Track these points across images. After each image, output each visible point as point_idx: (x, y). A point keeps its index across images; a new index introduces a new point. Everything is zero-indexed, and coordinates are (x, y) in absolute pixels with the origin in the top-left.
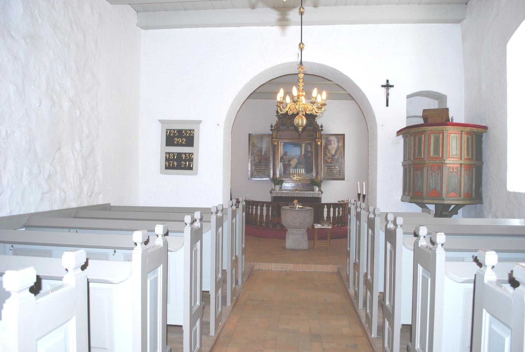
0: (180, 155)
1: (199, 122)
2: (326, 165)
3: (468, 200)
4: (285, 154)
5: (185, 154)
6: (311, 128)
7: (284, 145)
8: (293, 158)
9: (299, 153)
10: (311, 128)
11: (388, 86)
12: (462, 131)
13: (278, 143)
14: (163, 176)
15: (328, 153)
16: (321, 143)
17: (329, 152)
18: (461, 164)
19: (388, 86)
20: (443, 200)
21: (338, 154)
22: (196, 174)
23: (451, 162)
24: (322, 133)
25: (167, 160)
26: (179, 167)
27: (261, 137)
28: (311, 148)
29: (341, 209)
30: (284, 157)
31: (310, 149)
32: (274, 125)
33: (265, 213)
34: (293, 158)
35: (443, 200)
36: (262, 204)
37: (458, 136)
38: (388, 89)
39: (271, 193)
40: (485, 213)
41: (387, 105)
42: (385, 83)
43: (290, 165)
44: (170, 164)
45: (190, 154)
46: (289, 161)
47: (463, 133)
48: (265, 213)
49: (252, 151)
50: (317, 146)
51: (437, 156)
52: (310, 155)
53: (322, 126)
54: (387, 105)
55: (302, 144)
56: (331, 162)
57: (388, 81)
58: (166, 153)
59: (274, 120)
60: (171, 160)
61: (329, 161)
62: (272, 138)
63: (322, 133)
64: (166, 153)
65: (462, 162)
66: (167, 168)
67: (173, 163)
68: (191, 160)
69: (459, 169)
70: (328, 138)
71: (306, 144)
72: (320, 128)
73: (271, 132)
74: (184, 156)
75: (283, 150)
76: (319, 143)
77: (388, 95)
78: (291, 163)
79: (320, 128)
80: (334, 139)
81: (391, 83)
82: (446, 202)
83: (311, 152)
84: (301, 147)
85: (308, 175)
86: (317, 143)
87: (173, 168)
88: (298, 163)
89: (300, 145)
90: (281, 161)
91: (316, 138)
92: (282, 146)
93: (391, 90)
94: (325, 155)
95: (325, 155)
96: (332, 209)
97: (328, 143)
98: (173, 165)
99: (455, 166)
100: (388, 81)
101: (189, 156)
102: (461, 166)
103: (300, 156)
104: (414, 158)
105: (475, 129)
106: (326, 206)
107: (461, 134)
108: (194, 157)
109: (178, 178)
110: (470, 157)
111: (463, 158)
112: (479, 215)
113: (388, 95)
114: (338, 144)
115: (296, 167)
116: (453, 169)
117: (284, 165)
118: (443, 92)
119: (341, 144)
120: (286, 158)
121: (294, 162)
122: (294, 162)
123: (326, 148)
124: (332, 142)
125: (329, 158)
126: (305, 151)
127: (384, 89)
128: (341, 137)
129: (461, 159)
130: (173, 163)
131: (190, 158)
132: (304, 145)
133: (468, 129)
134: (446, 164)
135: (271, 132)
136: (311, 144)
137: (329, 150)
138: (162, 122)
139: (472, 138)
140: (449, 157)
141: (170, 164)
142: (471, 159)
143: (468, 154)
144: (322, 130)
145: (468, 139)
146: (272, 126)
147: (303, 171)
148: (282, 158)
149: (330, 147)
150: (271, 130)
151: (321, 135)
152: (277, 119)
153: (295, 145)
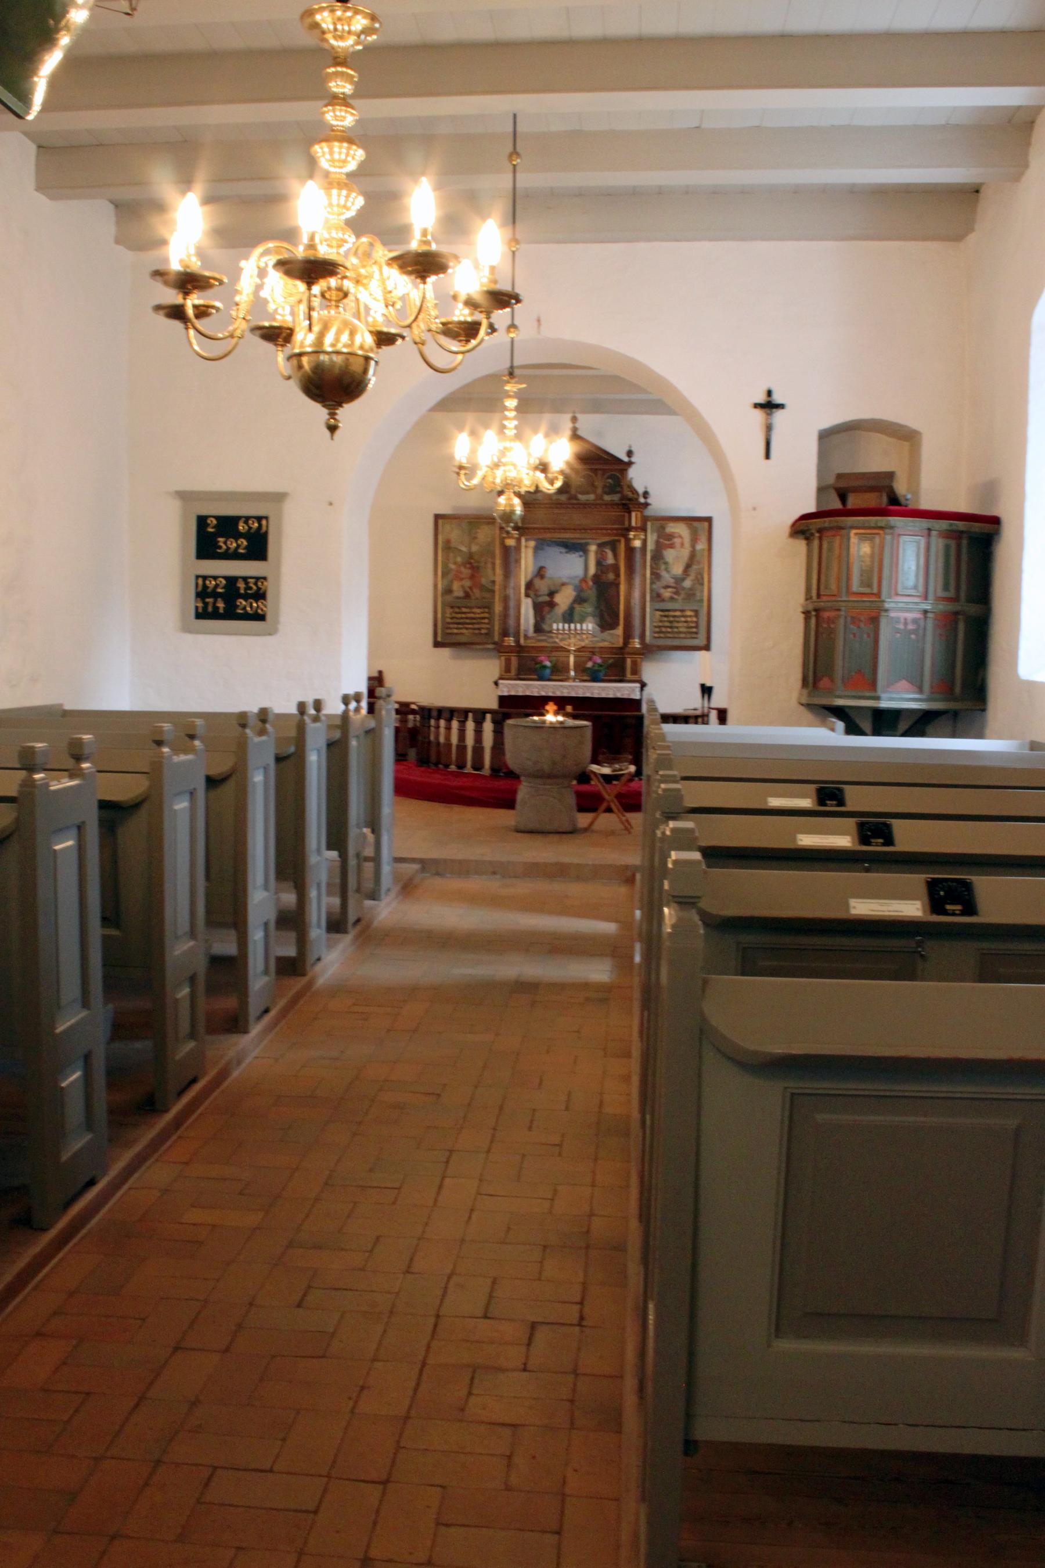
0: (232, 581)
1: (279, 498)
3: (943, 700)
4: (540, 573)
5: (245, 579)
6: (616, 498)
8: (563, 584)
10: (616, 498)
11: (769, 406)
12: (929, 530)
13: (519, 540)
14: (189, 637)
15: (664, 574)
16: (644, 542)
17: (667, 570)
18: (925, 612)
19: (769, 406)
20: (878, 698)
21: (692, 576)
22: (272, 632)
23: (901, 605)
24: (648, 512)
25: (202, 594)
26: (231, 614)
28: (616, 556)
30: (538, 583)
31: (610, 560)
33: (470, 741)
34: (563, 584)
35: (878, 698)
37: (923, 541)
38: (769, 415)
39: (496, 684)
40: (987, 732)
41: (768, 456)
42: (761, 398)
43: (552, 605)
44: (206, 604)
45: (257, 579)
46: (552, 594)
47: (934, 533)
49: (445, 565)
50: (630, 551)
52: (611, 576)
53: (646, 494)
54: (768, 456)
55: (587, 544)
56: (672, 598)
57: (769, 393)
58: (197, 577)
60: (209, 596)
61: (667, 594)
63: (648, 512)
64: (197, 577)
65: (928, 607)
66: (199, 616)
67: (215, 603)
68: (260, 596)
69: (922, 623)
70: (663, 528)
71: (600, 545)
74: (241, 585)
76: (637, 543)
77: (769, 428)
78: (558, 599)
79: (642, 500)
80: (681, 530)
81: (777, 398)
82: (884, 704)
83: (616, 568)
85: (606, 635)
86: (628, 541)
87: (215, 615)
88: (579, 600)
90: (527, 595)
91: (630, 529)
92: (530, 552)
93: (778, 415)
94: (656, 576)
95: (656, 576)
97: (666, 540)
98: (216, 608)
99: (910, 616)
100: (769, 393)
101: (256, 584)
102: (926, 618)
103: (584, 580)
104: (819, 596)
105: (961, 525)
107: (929, 535)
108: (270, 587)
109: (227, 645)
110: (951, 594)
111: (931, 596)
112: (980, 735)
113: (769, 428)
115: (569, 617)
116: (906, 624)
118: (913, 424)
120: (542, 586)
121: (564, 599)
122: (564, 599)
123: (657, 557)
124: (677, 541)
125: (667, 587)
126: (599, 563)
127: (759, 415)
129: (926, 598)
130: (215, 603)
131: (259, 589)
132: (593, 548)
133: (944, 525)
134: (886, 610)
136: (613, 546)
137: (666, 563)
138: (185, 497)
139: (959, 546)
140: (897, 594)
141: (206, 604)
142: (956, 599)
143: (946, 588)
144: (647, 505)
145: (947, 548)
147: (590, 626)
148: (529, 585)
149: (669, 555)
151: (645, 519)
153: (571, 547)
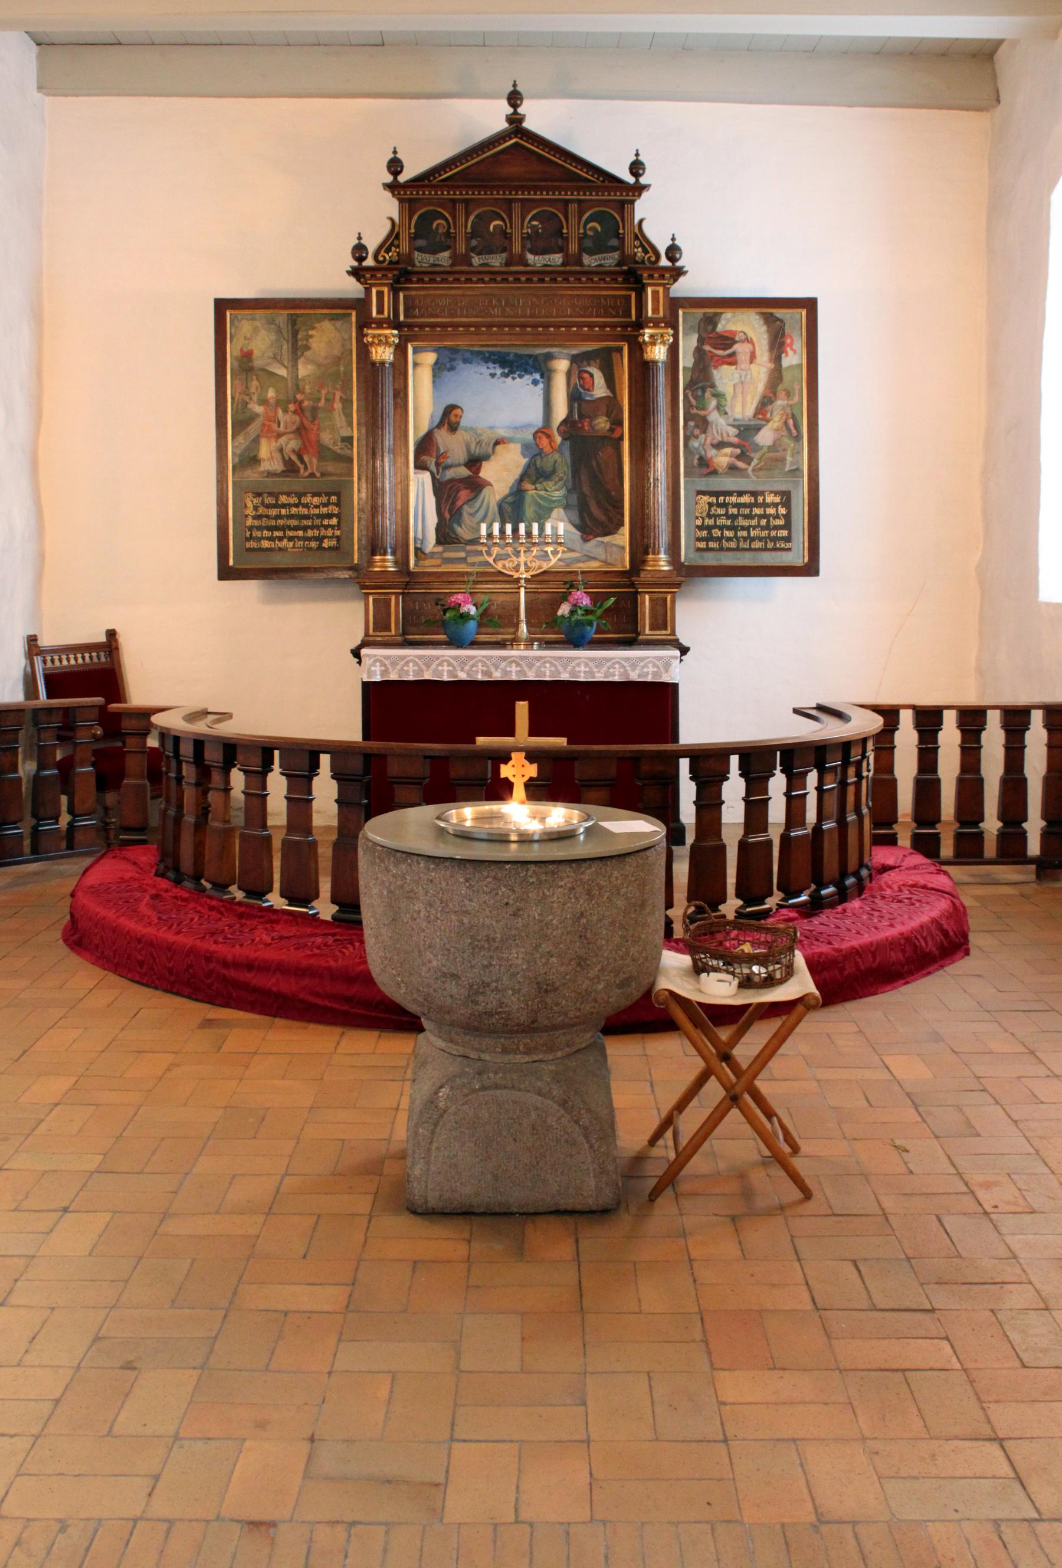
2: (703, 484)
4: (449, 418)
6: (610, 260)
7: (438, 369)
9: (536, 417)
10: (610, 260)
15: (714, 416)
16: (673, 350)
24: (682, 288)
27: (295, 314)
28: (611, 382)
29: (812, 778)
30: (443, 438)
31: (600, 389)
32: (372, 244)
33: (777, 812)
36: (302, 758)
43: (475, 486)
46: (474, 462)
48: (777, 812)
50: (643, 370)
51: (379, 289)
52: (602, 423)
53: (673, 251)
55: (550, 357)
56: (732, 468)
59: (377, 217)
61: (723, 459)
62: (365, 322)
71: (575, 359)
72: (664, 262)
73: (352, 288)
75: (435, 398)
76: (659, 353)
78: (487, 472)
80: (749, 326)
83: (611, 405)
84: (547, 376)
85: (594, 546)
88: (535, 472)
89: (538, 367)
91: (640, 325)
96: (778, 784)
103: (544, 431)
106: (734, 760)
114: (777, 360)
117: (440, 489)
119: (794, 358)
121: (501, 473)
122: (501, 473)
124: (741, 349)
125: (720, 445)
126: (574, 397)
128: (791, 318)
132: (562, 365)
135: (352, 288)
137: (718, 395)
144: (678, 273)
146: (359, 252)
149: (724, 377)
150: (356, 273)
152: (390, 207)
153: (513, 365)
